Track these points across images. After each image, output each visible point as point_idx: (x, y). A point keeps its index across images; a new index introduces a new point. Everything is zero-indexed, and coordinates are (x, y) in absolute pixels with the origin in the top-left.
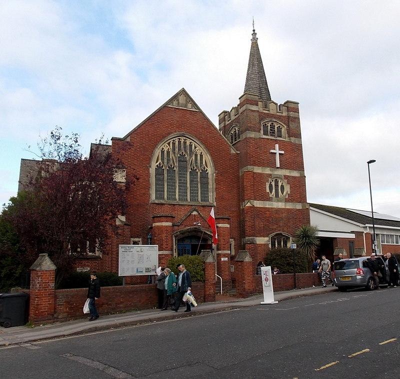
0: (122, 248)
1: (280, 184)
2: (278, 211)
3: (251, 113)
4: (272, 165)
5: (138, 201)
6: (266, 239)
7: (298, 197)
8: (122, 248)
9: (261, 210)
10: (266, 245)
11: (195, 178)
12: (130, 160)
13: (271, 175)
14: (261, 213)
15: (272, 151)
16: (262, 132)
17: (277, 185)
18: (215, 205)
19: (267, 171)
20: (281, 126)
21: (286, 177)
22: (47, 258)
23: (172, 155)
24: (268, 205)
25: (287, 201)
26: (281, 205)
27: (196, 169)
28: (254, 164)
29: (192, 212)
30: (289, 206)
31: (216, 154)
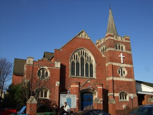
2: (122, 82)
15: (119, 56)
21: (126, 67)
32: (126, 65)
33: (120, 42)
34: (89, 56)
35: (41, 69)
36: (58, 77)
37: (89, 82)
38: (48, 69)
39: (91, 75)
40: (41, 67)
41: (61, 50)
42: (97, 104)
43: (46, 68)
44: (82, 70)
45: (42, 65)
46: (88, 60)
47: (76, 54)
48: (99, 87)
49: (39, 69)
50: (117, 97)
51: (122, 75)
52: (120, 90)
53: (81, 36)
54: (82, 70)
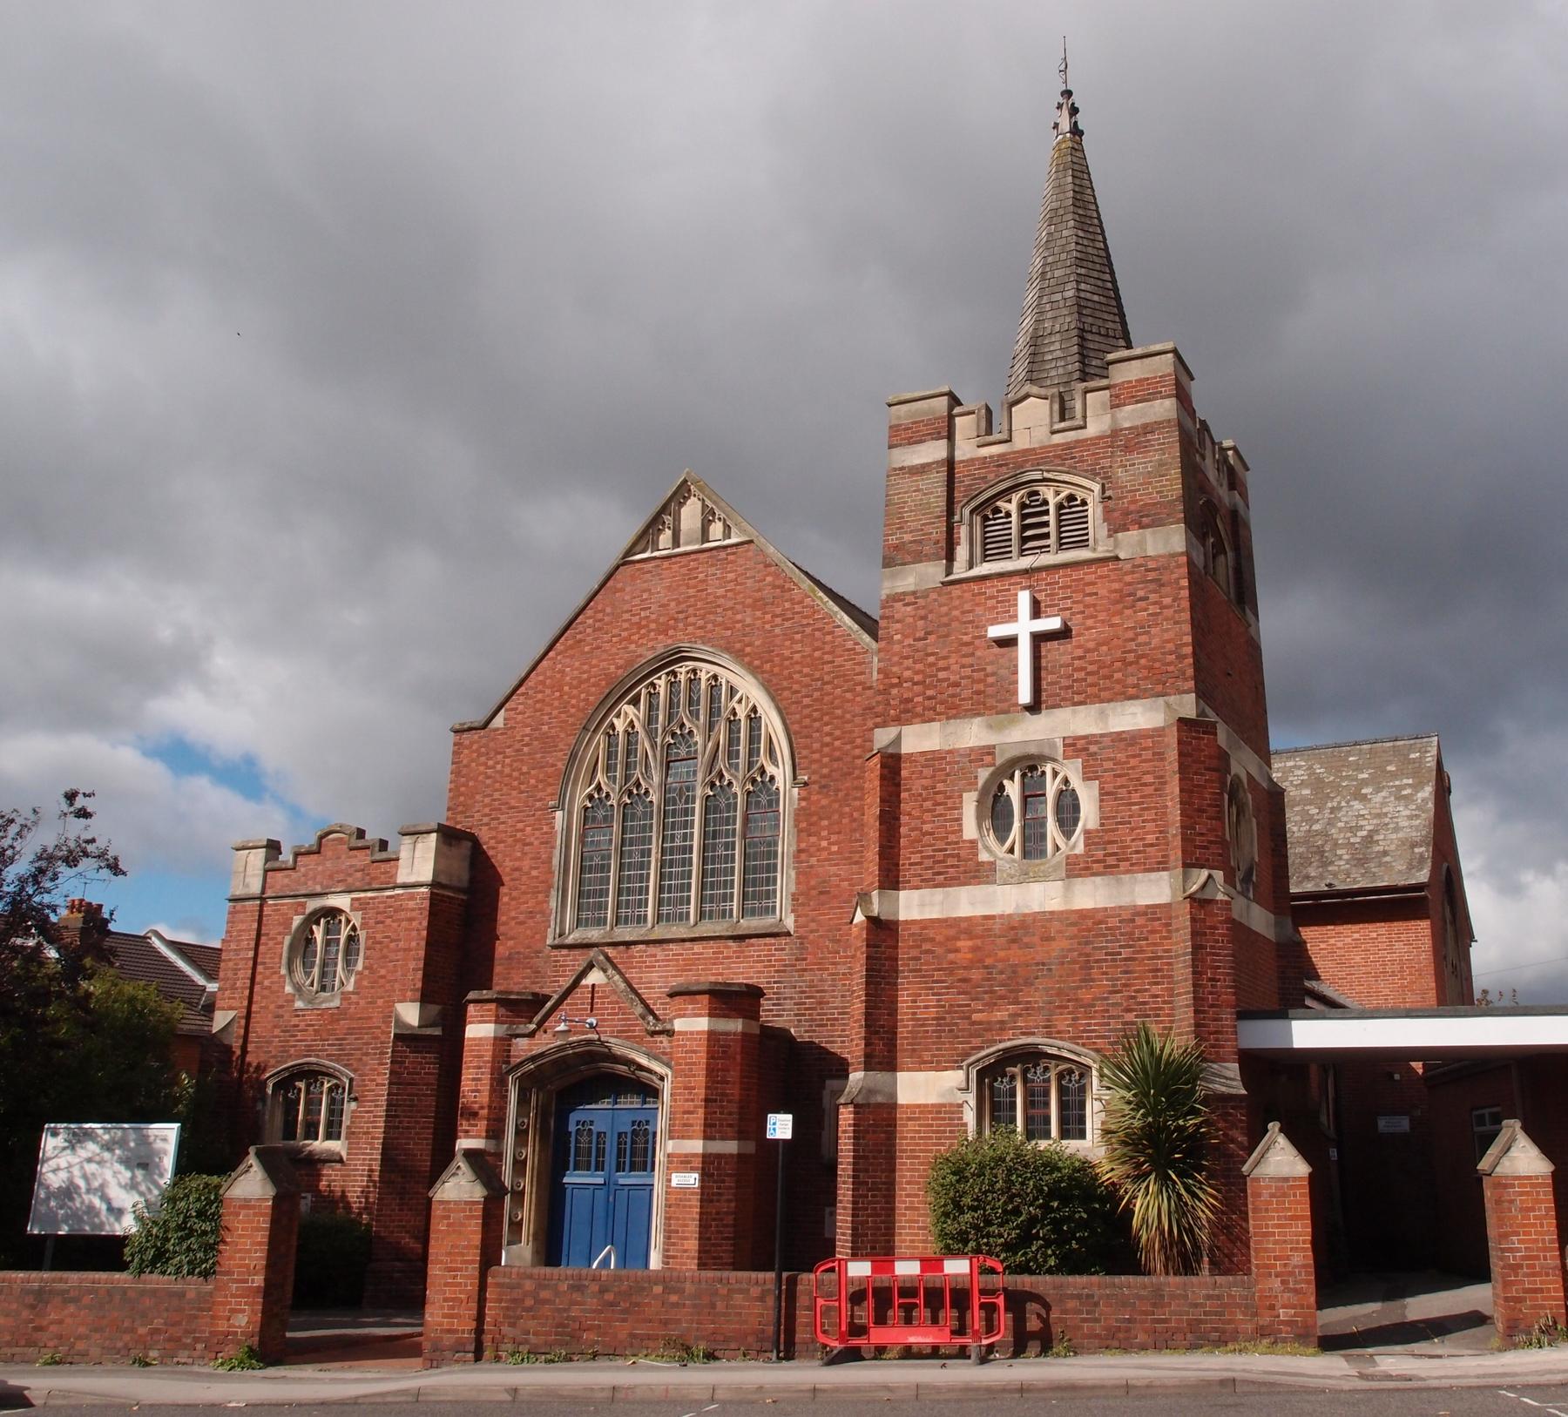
0: (790, 1117)
1: (1051, 788)
2: (1020, 929)
3: (907, 482)
4: (990, 699)
5: (510, 943)
6: (955, 1077)
7: (1151, 838)
8: (790, 1117)
9: (931, 933)
10: (946, 1113)
11: (727, 821)
12: (496, 795)
13: (989, 751)
14: (926, 946)
15: (995, 631)
16: (1045, 518)
17: (1032, 796)
18: (790, 923)
19: (972, 734)
20: (1080, 494)
21: (1077, 746)
22: (1282, 1140)
23: (644, 743)
24: (966, 902)
25: (1077, 869)
26: (1043, 896)
27: (730, 784)
28: (907, 714)
29: (583, 974)
30: (1091, 895)
31: (806, 701)
32: (1093, 709)
33: (1037, 464)
34: (742, 713)
35: (1007, 770)
36: (412, 965)
37: (595, 977)
38: (358, 905)
39: (758, 891)
40: (313, 905)
41: (498, 722)
42: (961, 1106)
43: (342, 901)
44: (673, 858)
45: (318, 889)
46: (732, 754)
47: (620, 725)
48: (679, 1025)
49: (297, 920)
50: (937, 1109)
51: (1033, 844)
52: (988, 1027)
53: (665, 538)
54: (673, 858)
